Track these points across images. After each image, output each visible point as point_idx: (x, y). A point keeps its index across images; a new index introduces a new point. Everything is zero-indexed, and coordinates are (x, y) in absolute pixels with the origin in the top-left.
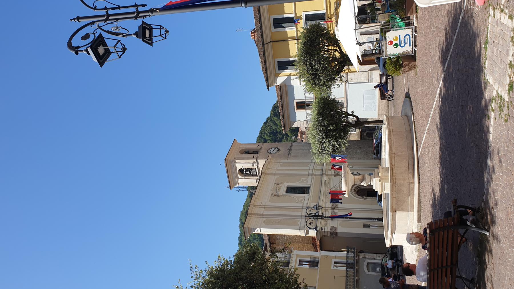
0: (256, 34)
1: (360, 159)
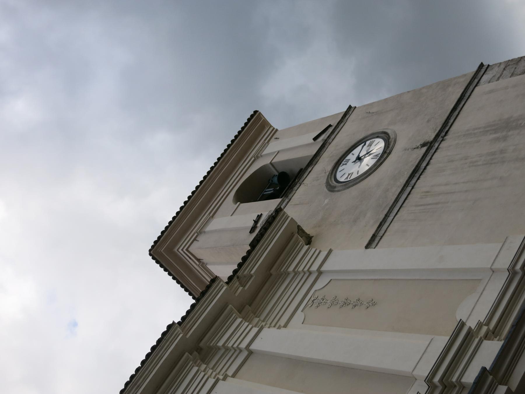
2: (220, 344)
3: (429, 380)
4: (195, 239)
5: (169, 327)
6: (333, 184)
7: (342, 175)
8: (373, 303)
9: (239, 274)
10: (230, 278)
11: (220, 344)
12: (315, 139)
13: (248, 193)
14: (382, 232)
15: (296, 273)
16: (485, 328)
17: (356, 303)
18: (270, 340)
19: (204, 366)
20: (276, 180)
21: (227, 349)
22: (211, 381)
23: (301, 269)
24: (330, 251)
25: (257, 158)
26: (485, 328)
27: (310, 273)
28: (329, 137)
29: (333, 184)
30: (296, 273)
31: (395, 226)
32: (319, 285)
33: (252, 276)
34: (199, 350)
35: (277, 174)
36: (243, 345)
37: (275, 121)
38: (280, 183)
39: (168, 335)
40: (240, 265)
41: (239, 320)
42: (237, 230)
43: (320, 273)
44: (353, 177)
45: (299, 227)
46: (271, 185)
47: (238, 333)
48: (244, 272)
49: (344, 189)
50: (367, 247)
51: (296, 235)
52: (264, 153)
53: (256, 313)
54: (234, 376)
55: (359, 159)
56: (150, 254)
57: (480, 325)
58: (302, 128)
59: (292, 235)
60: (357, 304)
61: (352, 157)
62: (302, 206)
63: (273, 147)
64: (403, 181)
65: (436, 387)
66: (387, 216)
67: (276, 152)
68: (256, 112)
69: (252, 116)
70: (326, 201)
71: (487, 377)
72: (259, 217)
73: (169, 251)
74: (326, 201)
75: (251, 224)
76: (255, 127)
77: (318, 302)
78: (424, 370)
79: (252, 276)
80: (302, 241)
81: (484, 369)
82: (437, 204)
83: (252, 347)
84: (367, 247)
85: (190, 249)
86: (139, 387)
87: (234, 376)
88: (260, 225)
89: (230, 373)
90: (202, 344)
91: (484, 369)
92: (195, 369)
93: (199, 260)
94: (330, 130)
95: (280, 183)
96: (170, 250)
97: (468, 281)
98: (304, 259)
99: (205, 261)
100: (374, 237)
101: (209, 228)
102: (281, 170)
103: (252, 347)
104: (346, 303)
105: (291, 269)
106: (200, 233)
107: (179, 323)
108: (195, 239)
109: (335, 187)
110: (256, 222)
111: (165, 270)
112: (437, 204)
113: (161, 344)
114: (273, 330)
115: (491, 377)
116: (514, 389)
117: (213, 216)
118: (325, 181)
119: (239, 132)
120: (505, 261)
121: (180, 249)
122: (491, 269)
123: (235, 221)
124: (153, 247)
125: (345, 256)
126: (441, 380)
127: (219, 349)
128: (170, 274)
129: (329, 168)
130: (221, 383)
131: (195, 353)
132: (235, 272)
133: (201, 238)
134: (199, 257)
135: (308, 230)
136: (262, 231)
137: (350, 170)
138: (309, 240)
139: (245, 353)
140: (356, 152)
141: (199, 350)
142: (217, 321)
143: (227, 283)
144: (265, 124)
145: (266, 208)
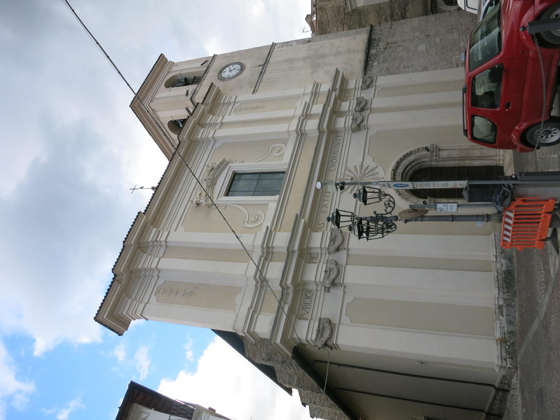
0: (426, 152)
1: (426, 69)
30: (224, 103)
31: (260, 88)
43: (235, 102)
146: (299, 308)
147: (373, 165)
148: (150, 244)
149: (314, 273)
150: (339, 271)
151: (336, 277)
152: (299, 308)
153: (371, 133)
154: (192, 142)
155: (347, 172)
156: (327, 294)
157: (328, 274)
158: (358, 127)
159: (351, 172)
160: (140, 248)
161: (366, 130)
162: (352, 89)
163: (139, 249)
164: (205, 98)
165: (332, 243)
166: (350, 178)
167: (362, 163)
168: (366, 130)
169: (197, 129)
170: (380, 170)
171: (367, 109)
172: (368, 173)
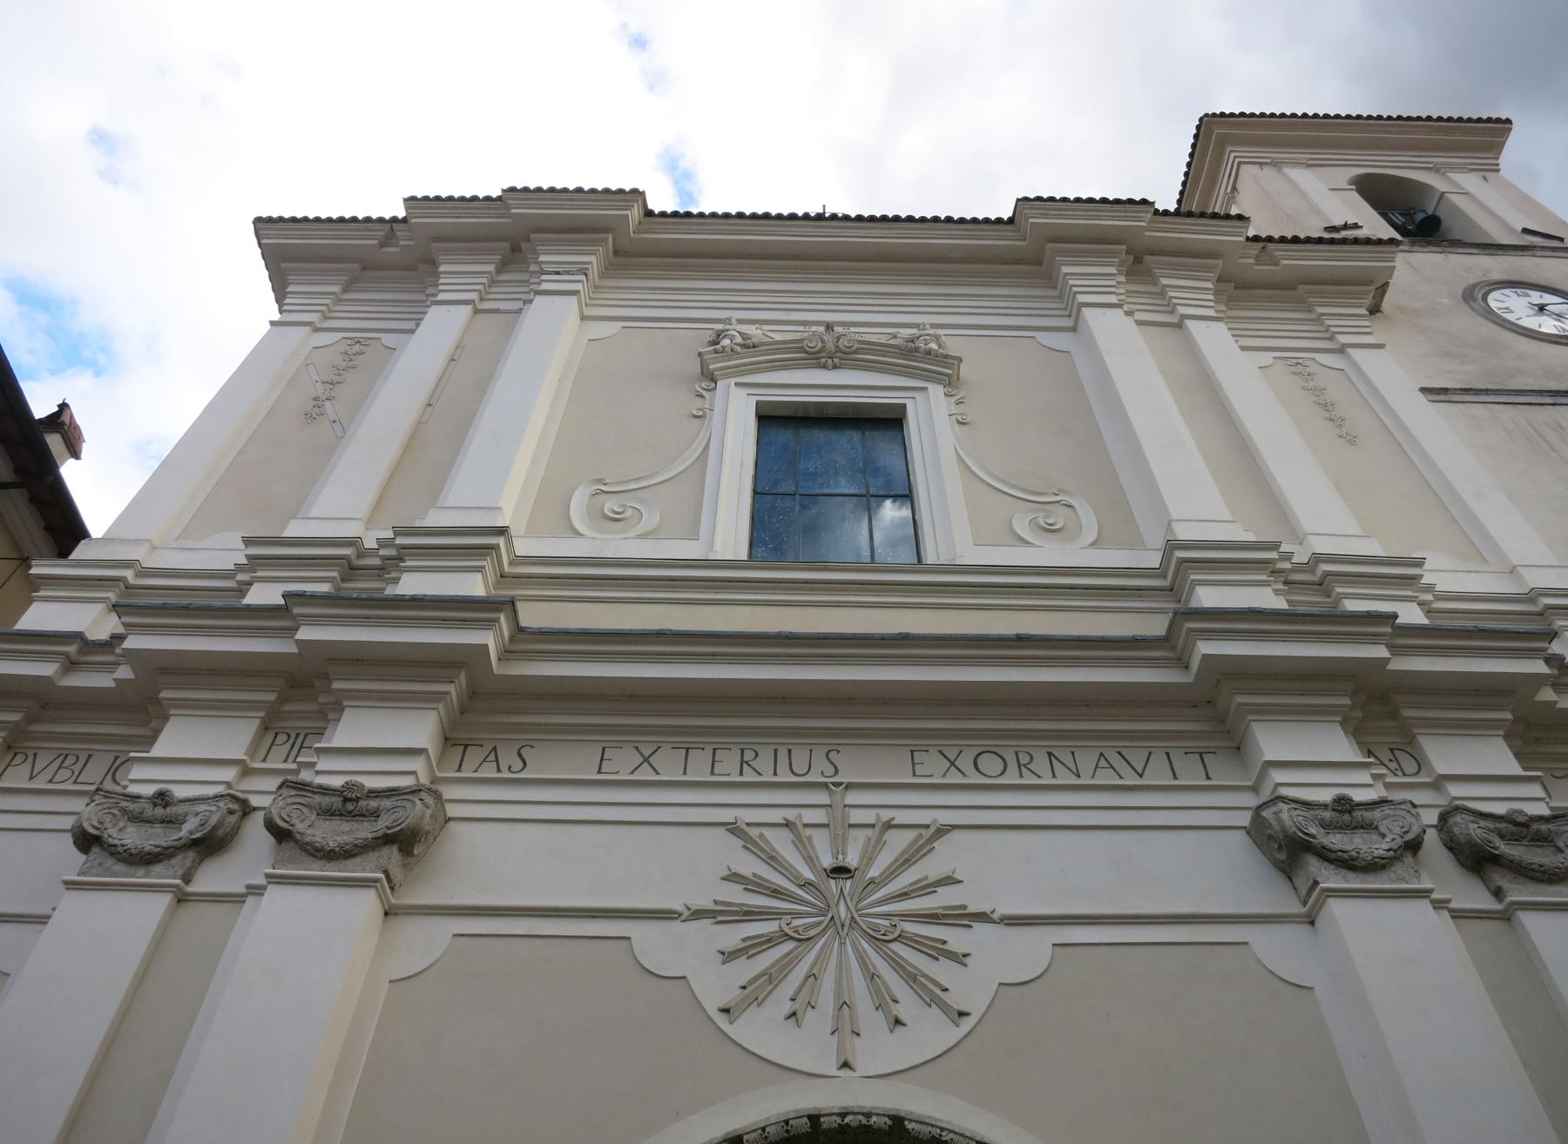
2: (1164, 281)
3: (1318, 558)
4: (1261, 164)
5: (1144, 202)
6: (1475, 296)
7: (1496, 300)
8: (1351, 440)
9: (1271, 246)
10: (1256, 239)
11: (1164, 281)
12: (1526, 231)
13: (1375, 191)
14: (1458, 398)
15: (1319, 319)
16: (1429, 597)
17: (1336, 420)
18: (1214, 339)
19: (1122, 279)
20: (1420, 217)
21: (1162, 294)
22: (1113, 299)
23: (1329, 323)
24: (1381, 346)
25: (1436, 169)
26: (1429, 597)
27: (1331, 339)
28: (1543, 248)
29: (1475, 296)
30: (1319, 319)
31: (1480, 410)
32: (1321, 357)
33: (1277, 264)
34: (1138, 260)
35: (1430, 212)
36: (1182, 310)
37: (1514, 153)
38: (1422, 224)
39: (1133, 207)
40: (1283, 240)
41: (1209, 285)
42: (1317, 211)
43: (1341, 350)
44: (1509, 317)
45: (1387, 284)
46: (1408, 214)
47: (1192, 294)
48: (1277, 250)
49: (1480, 314)
50: (1423, 390)
51: (1373, 288)
52: (1451, 175)
53: (1231, 302)
54: (1139, 323)
55: (1541, 308)
56: (1201, 120)
57: (1429, 588)
58: (1527, 203)
59: (1369, 283)
60: (1337, 421)
61: (1537, 297)
62: (1417, 272)
63: (1469, 181)
64: (1554, 386)
65: (1313, 572)
66: (1487, 391)
67: (1461, 189)
68: (1508, 121)
69: (1498, 120)
70: (1445, 301)
71: (1385, 625)
72: (1356, 226)
73: (1220, 138)
74: (1445, 301)
75: (1339, 222)
76: (1483, 137)
77: (1299, 369)
78: (1323, 546)
79: (1277, 264)
80: (1368, 301)
81: (1395, 616)
82: (1554, 449)
83: (1189, 323)
84: (1423, 390)
85: (1243, 167)
86: (1046, 216)
87: (1139, 323)
88: (1344, 234)
89: (1138, 316)
90: (1147, 258)
91: (1395, 616)
92: (1113, 270)
93: (1234, 188)
94: (1555, 244)
95: (1422, 224)
96: (1224, 142)
97: (1475, 543)
98: (1345, 319)
99: (1239, 198)
100: (1445, 391)
101: (1287, 170)
102: (1441, 213)
103: (1189, 323)
104: (1326, 407)
105: (1321, 310)
106: (1276, 164)
107: (1156, 212)
108: (1261, 164)
109: (1475, 300)
110: (1346, 227)
111: (1191, 155)
112: (1554, 449)
113: (1116, 207)
114: (1228, 334)
115: (1389, 630)
116: (1392, 666)
117: (1309, 166)
118: (1472, 281)
119: (1460, 120)
120: (1538, 579)
121: (1233, 155)
122: (1514, 567)
123: (1322, 197)
124: (1214, 115)
125: (1390, 369)
126: (1327, 574)
127: (1155, 284)
128: (1189, 165)
129: (1496, 276)
130: (1120, 312)
131: (1131, 258)
132: (1270, 239)
133: (1268, 172)
134: (1239, 186)
135: (1386, 305)
136: (1337, 238)
137: (1515, 306)
138: (1374, 310)
139: (1174, 320)
140: (1548, 298)
141: (1138, 260)
142: (1188, 257)
143: (1248, 239)
144: (1496, 147)
145: (1375, 226)
146: (64, 737)
147: (970, 988)
148: (533, 268)
149: (197, 754)
150: (1374, 867)
151: (1348, 863)
152: (64, 737)
153: (1268, 944)
154: (1039, 262)
155: (897, 842)
156: (68, 839)
157: (149, 812)
158: (1292, 849)
159: (905, 861)
160: (515, 249)
161: (1295, 907)
162: (1421, 764)
163: (506, 245)
164: (1296, 240)
165: (336, 802)
166: (852, 860)
167: (983, 917)
168: (1295, 907)
169: (1114, 254)
170: (929, 1034)
171: (1498, 894)
172: (898, 965)
